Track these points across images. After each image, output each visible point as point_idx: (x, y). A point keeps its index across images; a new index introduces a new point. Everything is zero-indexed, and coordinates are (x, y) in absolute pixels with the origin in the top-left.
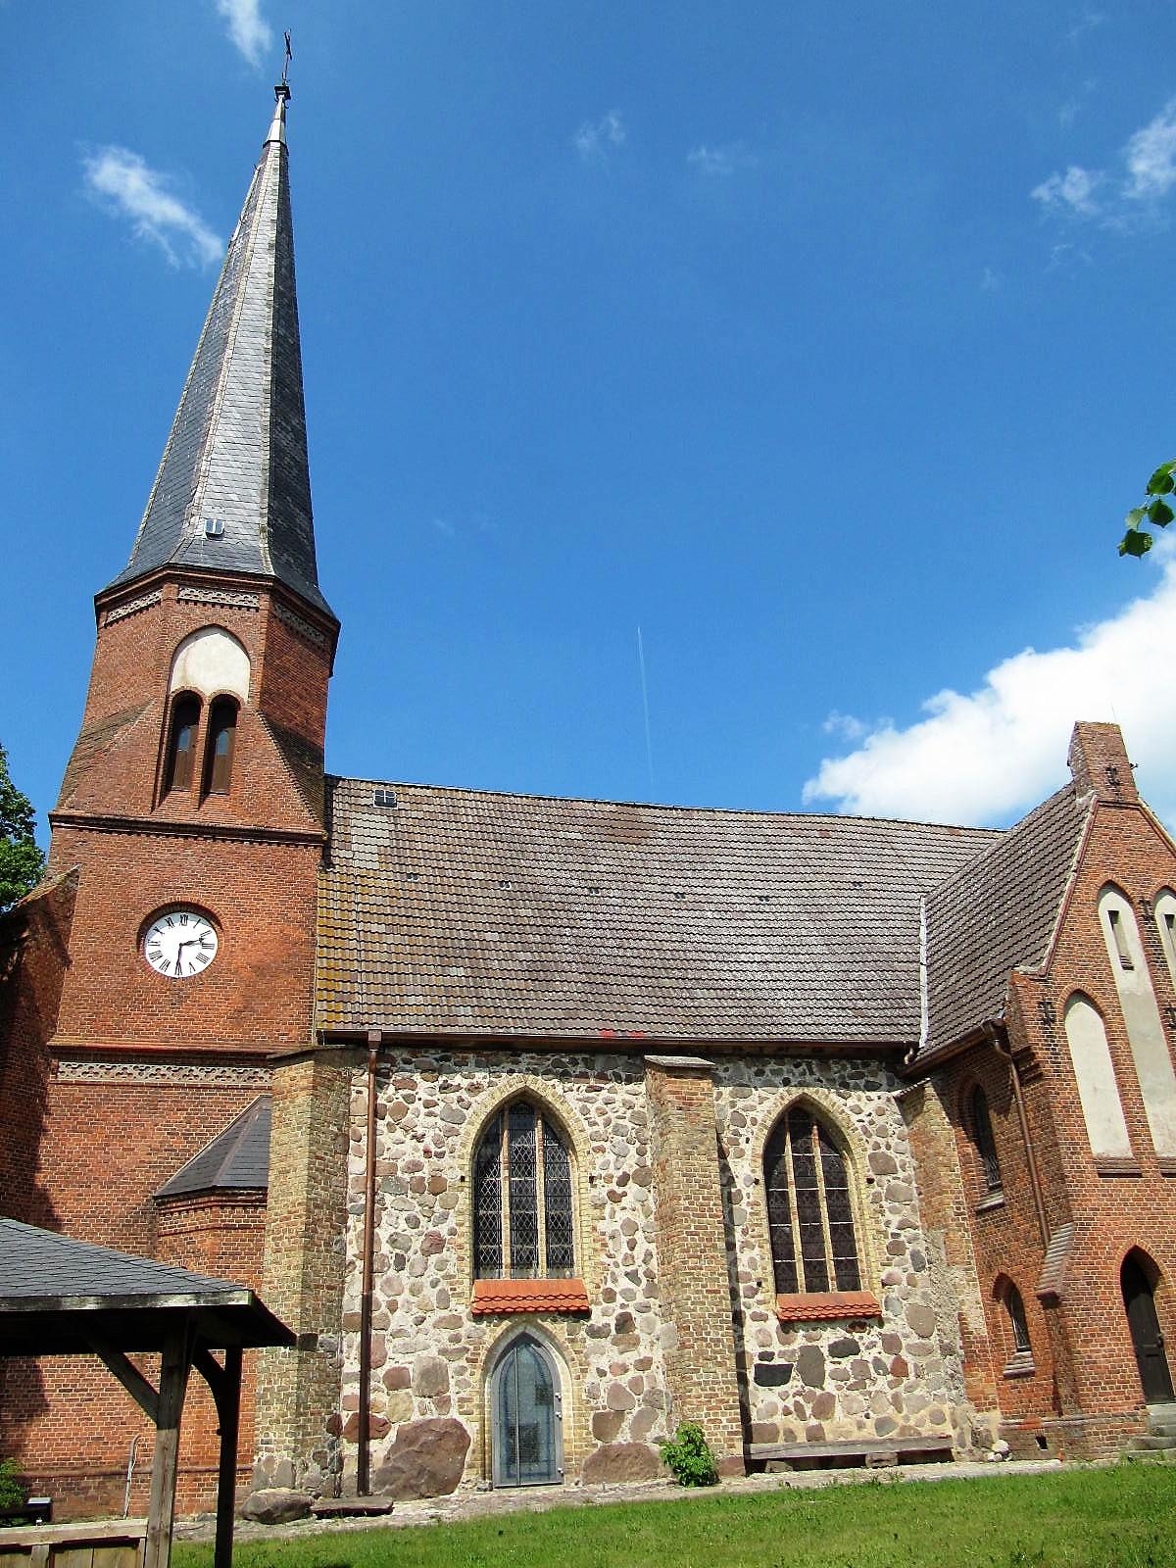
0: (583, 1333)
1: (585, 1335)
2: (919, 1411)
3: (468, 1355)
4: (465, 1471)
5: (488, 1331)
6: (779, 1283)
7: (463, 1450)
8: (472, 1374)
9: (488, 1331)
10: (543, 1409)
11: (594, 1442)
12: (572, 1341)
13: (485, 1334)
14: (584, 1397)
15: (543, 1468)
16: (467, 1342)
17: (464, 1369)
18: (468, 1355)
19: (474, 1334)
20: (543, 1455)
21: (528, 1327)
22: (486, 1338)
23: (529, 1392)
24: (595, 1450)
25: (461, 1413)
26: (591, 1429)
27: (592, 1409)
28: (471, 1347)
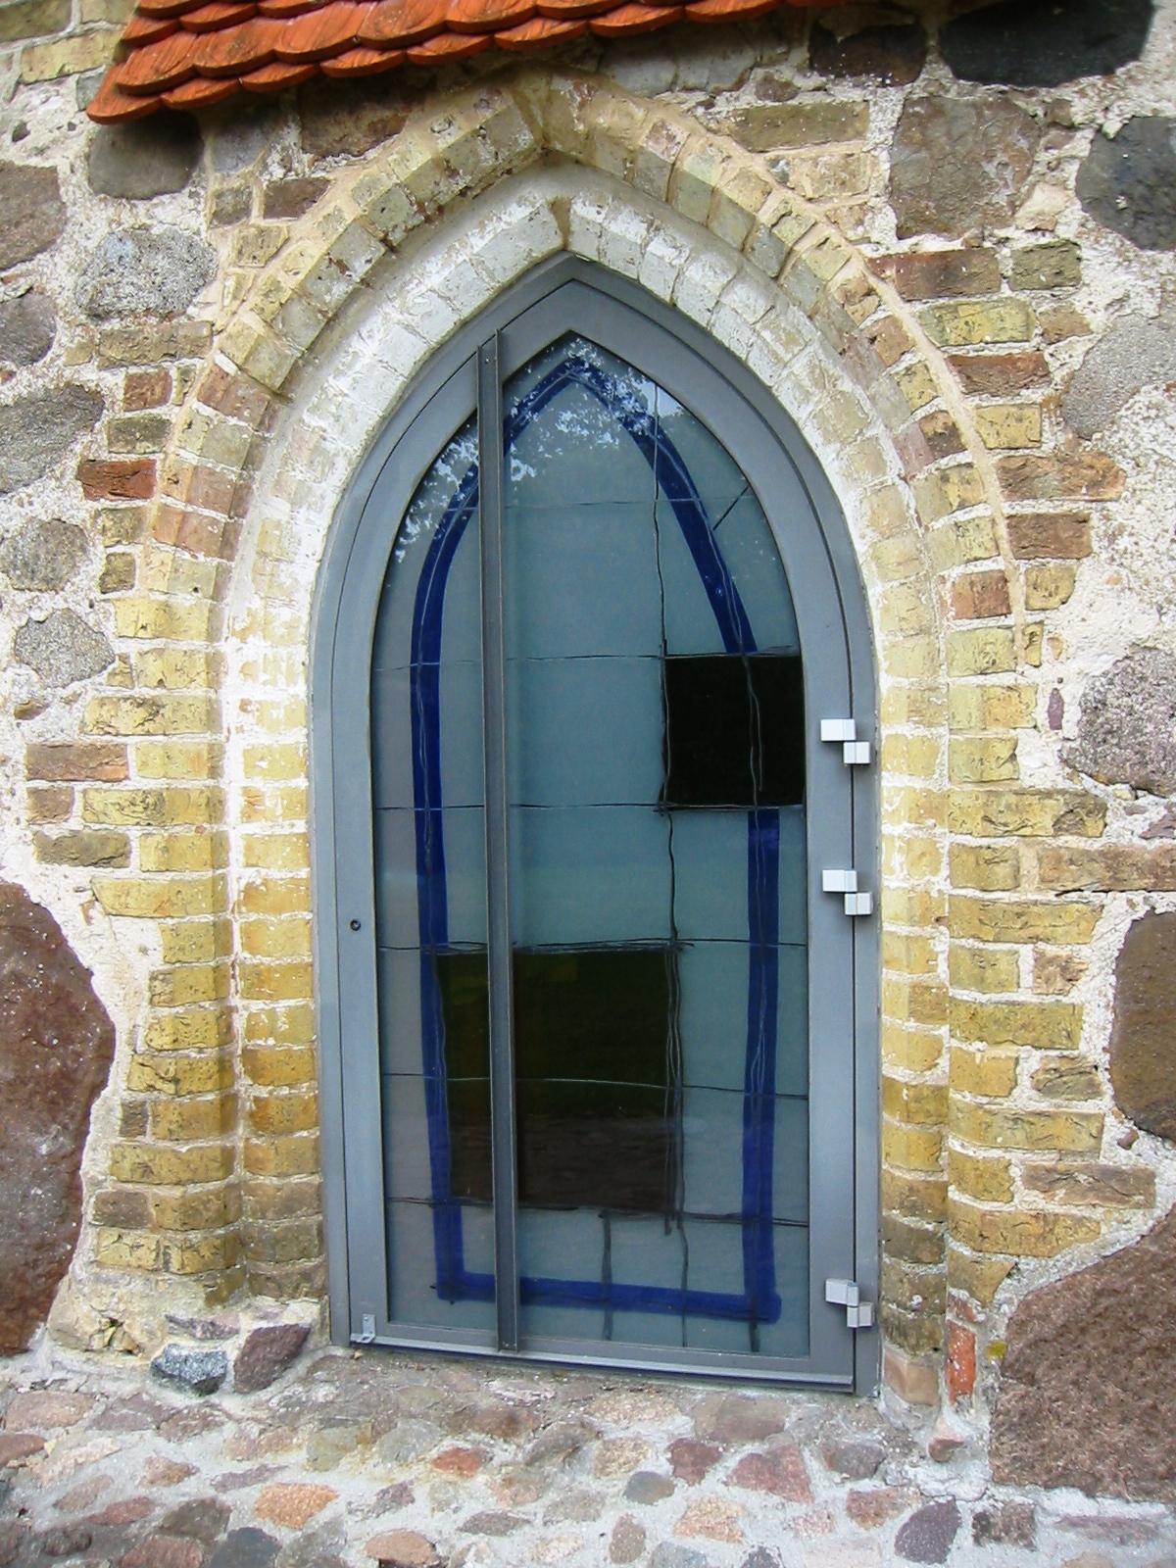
0: (1053, 203)
1: (1072, 219)
2: (1109, 782)
3: (95, 444)
4: (88, 1238)
5: (225, 252)
6: (397, 1208)
7: (66, 1097)
8: (118, 578)
9: (225, 252)
10: (720, 840)
11: (1114, 1157)
12: (941, 278)
13: (204, 278)
14: (1040, 762)
15: (720, 1266)
16: (89, 350)
17: (63, 536)
18: (95, 444)
19: (131, 291)
20: (712, 1172)
21: (583, 210)
22: (210, 307)
23: (620, 733)
24: (1125, 1228)
25: (53, 852)
26: (1095, 1039)
27: (1115, 869)
28: (113, 383)
